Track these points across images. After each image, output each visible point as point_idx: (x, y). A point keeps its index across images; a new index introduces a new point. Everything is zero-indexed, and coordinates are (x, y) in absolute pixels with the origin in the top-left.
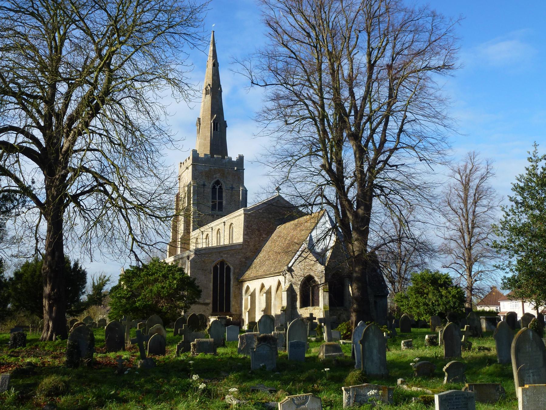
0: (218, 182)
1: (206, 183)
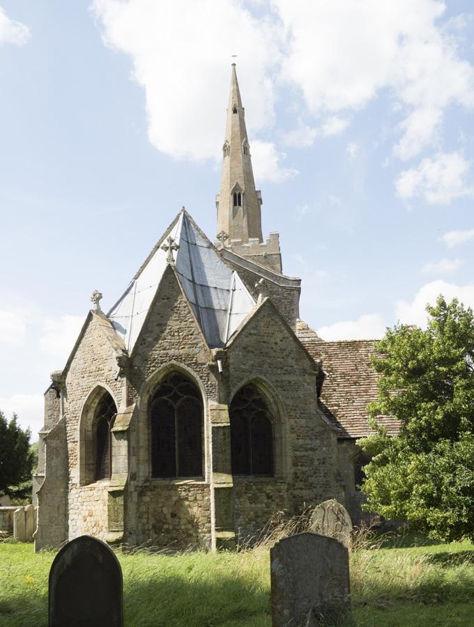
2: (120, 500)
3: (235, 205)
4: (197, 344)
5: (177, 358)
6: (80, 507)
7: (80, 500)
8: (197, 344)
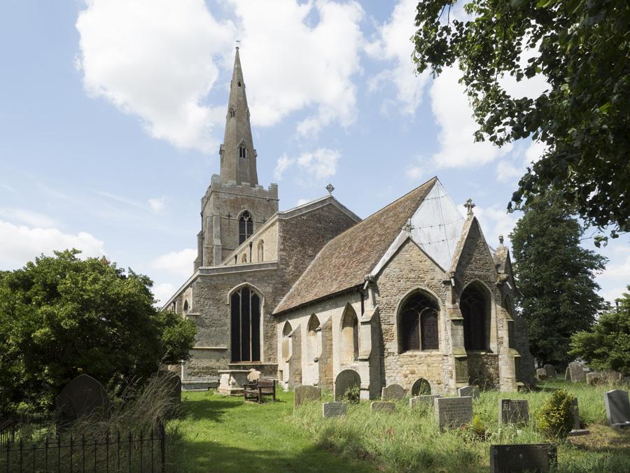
0: (246, 214)
1: (231, 214)
2: (465, 363)
3: (241, 156)
4: (490, 269)
5: (480, 277)
6: (400, 368)
7: (398, 363)
8: (490, 269)
